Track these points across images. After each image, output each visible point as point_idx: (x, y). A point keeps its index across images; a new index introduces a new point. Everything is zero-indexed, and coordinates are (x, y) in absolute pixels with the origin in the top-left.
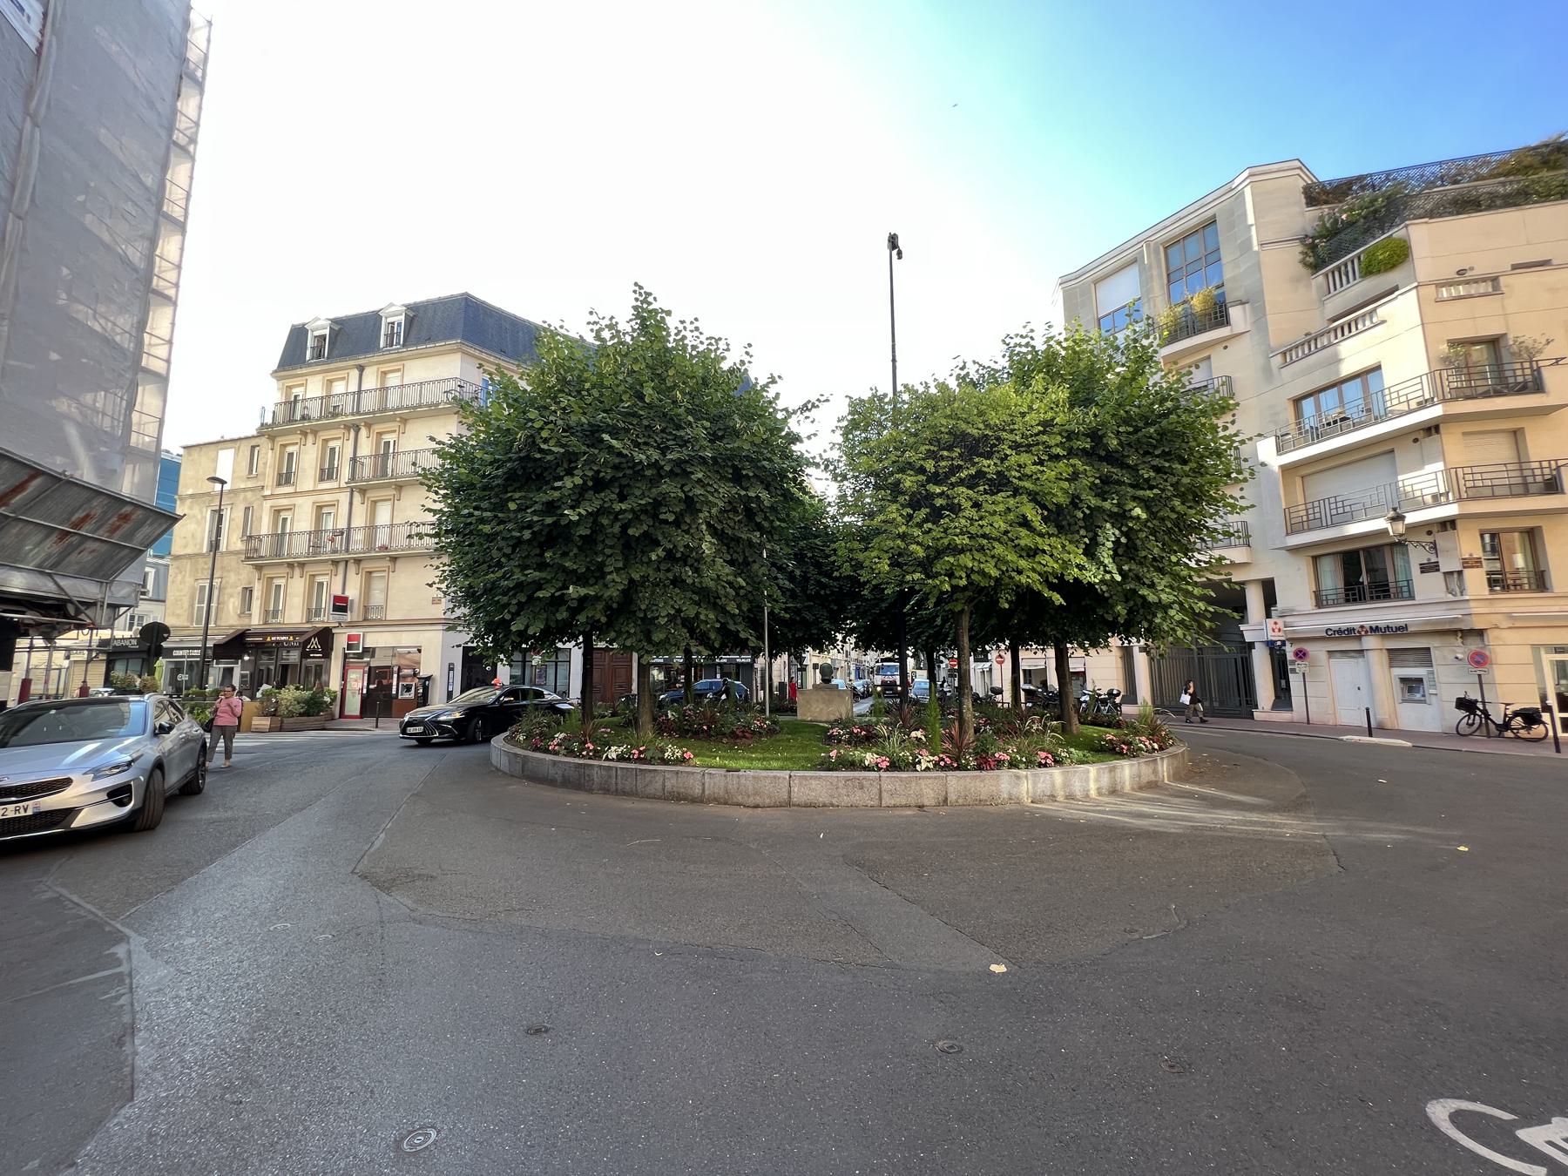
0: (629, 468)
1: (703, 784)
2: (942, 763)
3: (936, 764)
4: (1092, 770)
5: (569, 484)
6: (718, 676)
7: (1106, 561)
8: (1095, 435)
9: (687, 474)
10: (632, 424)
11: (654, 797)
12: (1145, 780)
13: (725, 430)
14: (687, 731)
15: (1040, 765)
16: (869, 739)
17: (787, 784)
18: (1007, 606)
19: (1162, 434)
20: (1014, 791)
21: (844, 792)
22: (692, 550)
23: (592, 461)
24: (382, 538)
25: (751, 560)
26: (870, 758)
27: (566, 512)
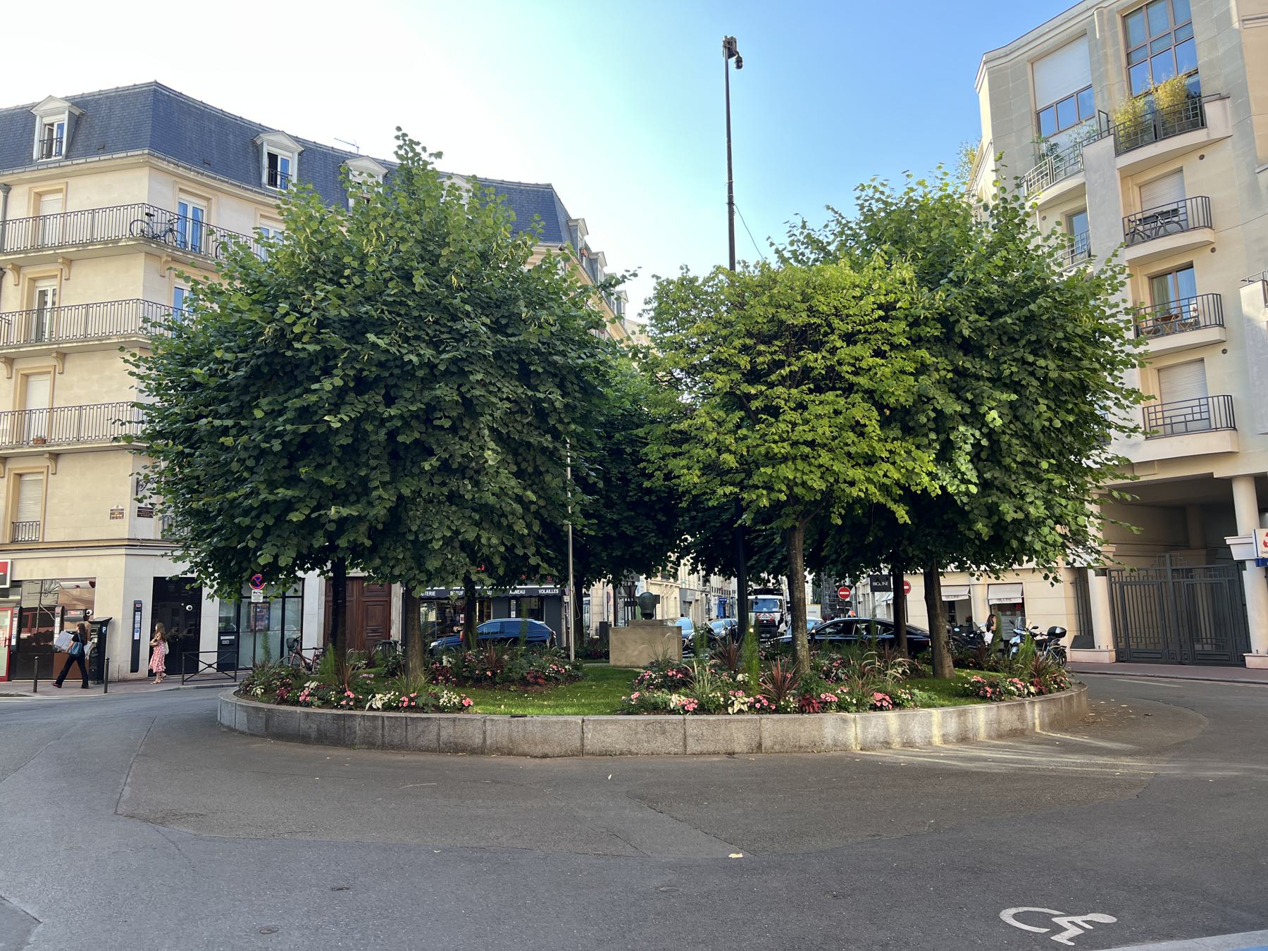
0: (397, 367)
1: (484, 732)
2: (758, 705)
3: (751, 707)
4: (936, 714)
5: (328, 387)
6: (513, 614)
7: (963, 469)
8: (946, 320)
9: (464, 374)
10: (399, 315)
11: (428, 750)
12: (1006, 727)
13: (509, 317)
14: (467, 679)
15: (874, 708)
16: (682, 683)
17: (579, 730)
18: (839, 522)
19: (1030, 320)
20: (840, 737)
21: (644, 737)
22: (471, 460)
23: (354, 358)
24: (38, 427)
25: (542, 469)
26: (675, 700)
27: (326, 418)
